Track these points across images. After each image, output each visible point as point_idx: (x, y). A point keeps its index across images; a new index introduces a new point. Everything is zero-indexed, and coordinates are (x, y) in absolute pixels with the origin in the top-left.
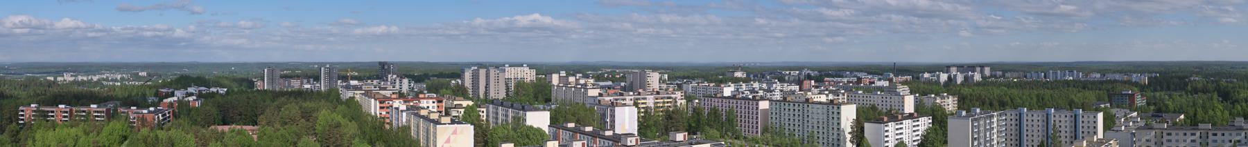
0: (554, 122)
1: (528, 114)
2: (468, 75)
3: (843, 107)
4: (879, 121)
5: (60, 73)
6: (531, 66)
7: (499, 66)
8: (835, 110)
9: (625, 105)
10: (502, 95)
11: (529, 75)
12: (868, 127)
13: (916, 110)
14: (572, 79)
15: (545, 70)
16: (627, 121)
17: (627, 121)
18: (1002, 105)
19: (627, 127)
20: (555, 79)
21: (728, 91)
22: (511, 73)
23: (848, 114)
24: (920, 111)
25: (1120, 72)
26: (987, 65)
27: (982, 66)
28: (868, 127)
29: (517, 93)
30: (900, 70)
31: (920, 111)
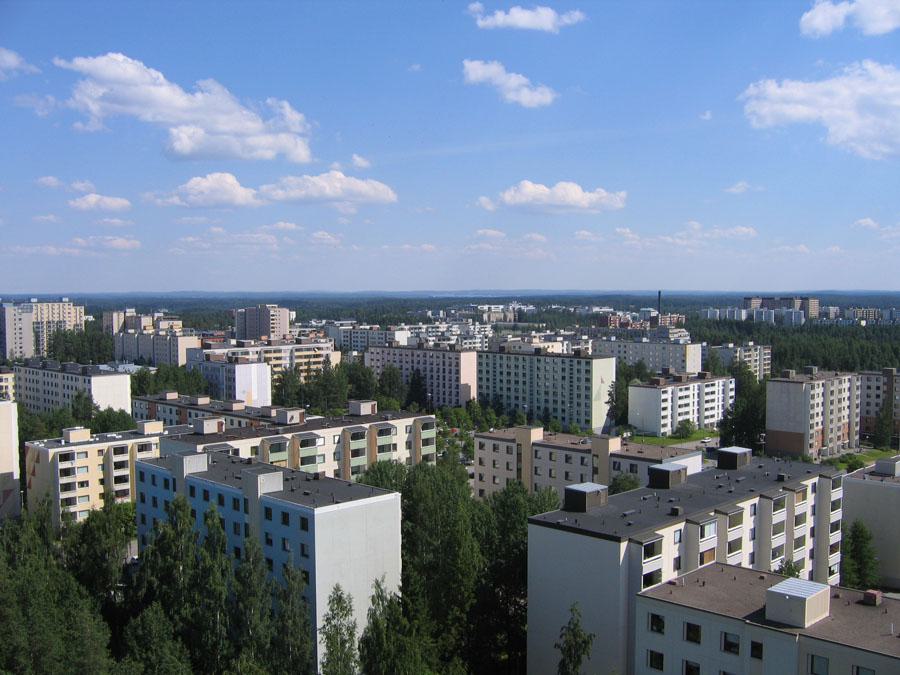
0: (139, 387)
1: (94, 380)
2: (798, 303)
3: (596, 363)
4: (654, 383)
5: (550, 304)
6: (77, 301)
7: (21, 301)
8: (583, 367)
9: (247, 362)
10: (29, 352)
11: (74, 318)
12: (636, 394)
13: (705, 367)
14: (146, 321)
15: (98, 308)
16: (254, 387)
17: (254, 387)
18: (847, 367)
19: (255, 397)
20: (117, 320)
21: (402, 336)
22: (47, 313)
23: (604, 373)
24: (711, 368)
25: (560, 303)
26: (815, 296)
27: (805, 298)
28: (636, 394)
29: (52, 348)
30: (662, 302)
31: (711, 368)
